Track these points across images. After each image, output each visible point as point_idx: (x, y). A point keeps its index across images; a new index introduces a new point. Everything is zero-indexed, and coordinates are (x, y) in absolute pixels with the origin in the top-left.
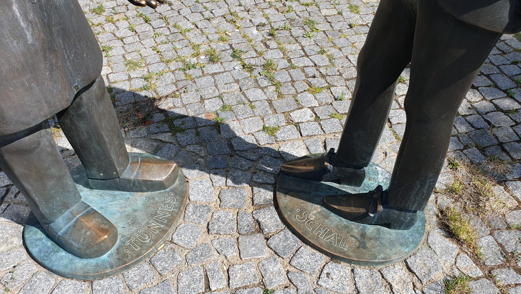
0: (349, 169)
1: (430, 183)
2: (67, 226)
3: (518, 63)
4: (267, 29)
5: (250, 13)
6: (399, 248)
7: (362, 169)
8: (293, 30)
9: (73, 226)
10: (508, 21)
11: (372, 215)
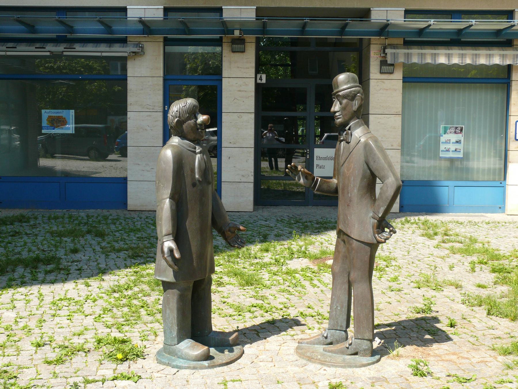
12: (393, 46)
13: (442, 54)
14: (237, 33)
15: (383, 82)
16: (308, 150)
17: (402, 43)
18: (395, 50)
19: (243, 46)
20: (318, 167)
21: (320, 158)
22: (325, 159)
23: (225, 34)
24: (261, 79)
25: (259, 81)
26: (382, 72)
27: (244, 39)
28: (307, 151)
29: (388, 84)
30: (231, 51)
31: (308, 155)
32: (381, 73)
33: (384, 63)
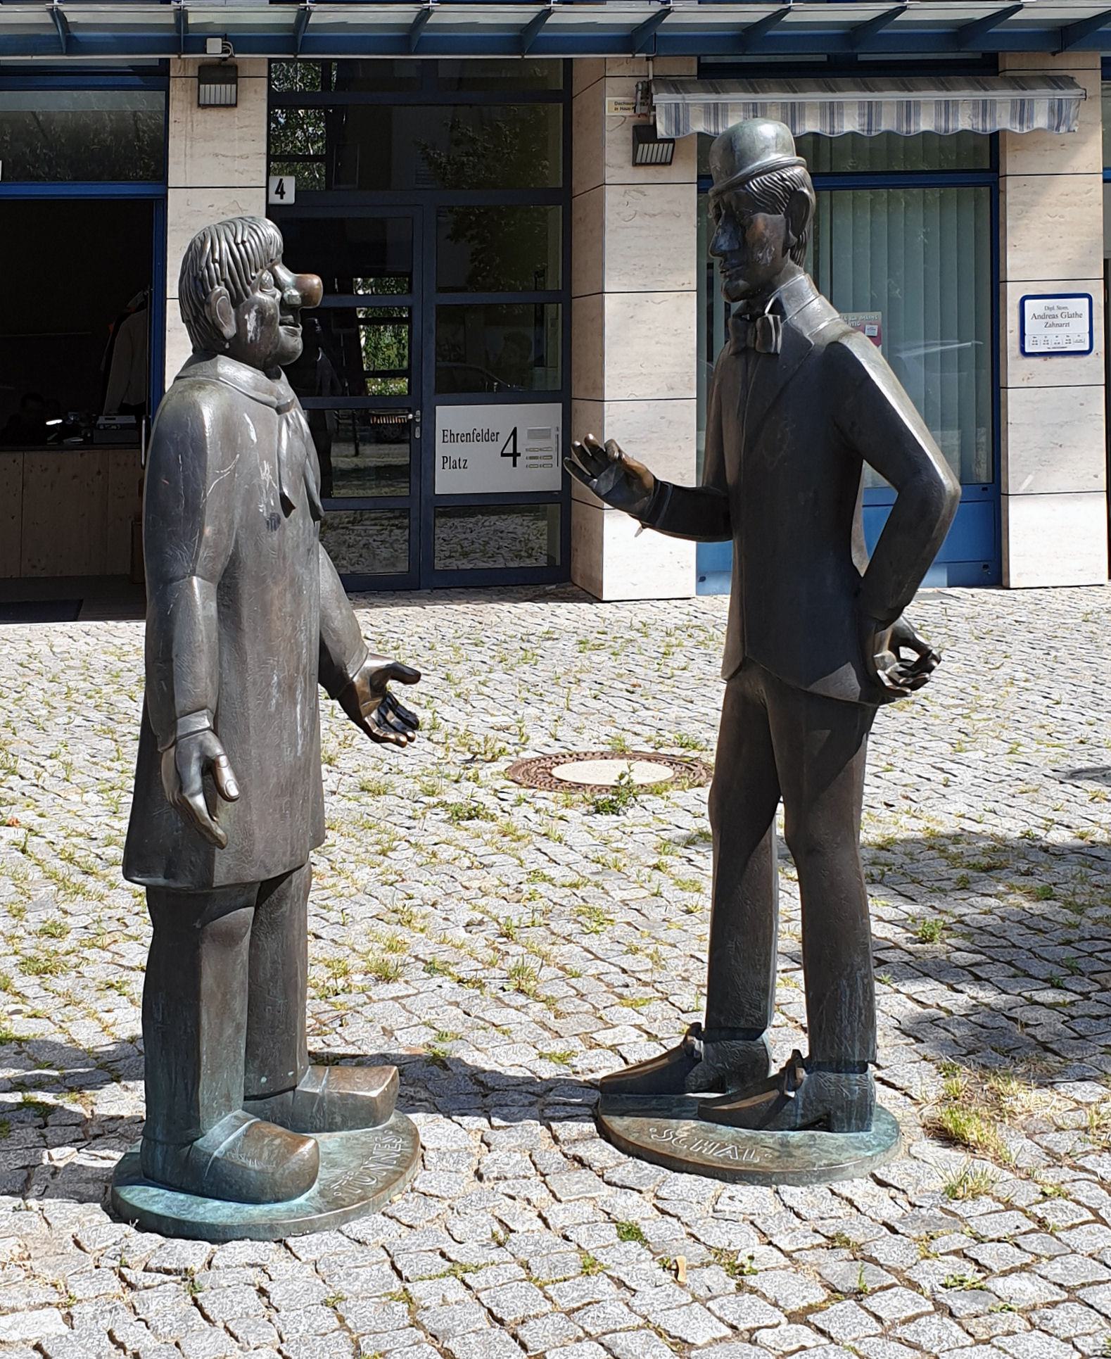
0: (734, 1043)
1: (862, 979)
2: (231, 1138)
3: (1072, 942)
4: (492, 928)
5: (439, 907)
6: (854, 1152)
7: (759, 1040)
8: (552, 925)
9: (245, 1136)
10: (859, 688)
11: (792, 1094)
12: (675, 84)
13: (927, 103)
14: (215, 48)
15: (642, 193)
16: (418, 413)
17: (695, 72)
18: (679, 96)
19: (230, 88)
20: (447, 465)
21: (454, 437)
22: (467, 438)
23: (177, 51)
24: (280, 191)
25: (276, 199)
26: (638, 160)
27: (236, 67)
28: (414, 414)
29: (656, 198)
30: (195, 104)
31: (418, 429)
32: (635, 164)
33: (644, 133)
